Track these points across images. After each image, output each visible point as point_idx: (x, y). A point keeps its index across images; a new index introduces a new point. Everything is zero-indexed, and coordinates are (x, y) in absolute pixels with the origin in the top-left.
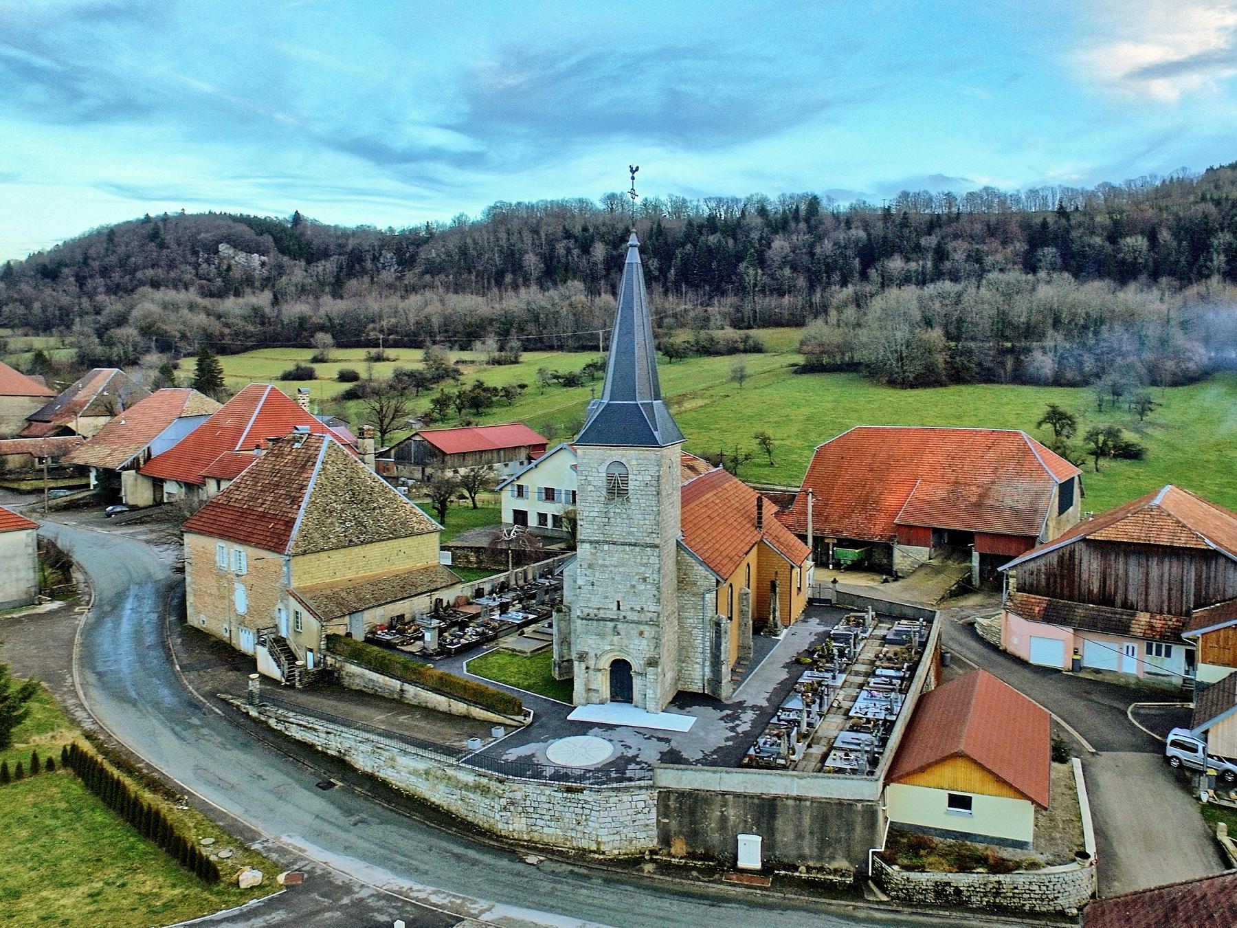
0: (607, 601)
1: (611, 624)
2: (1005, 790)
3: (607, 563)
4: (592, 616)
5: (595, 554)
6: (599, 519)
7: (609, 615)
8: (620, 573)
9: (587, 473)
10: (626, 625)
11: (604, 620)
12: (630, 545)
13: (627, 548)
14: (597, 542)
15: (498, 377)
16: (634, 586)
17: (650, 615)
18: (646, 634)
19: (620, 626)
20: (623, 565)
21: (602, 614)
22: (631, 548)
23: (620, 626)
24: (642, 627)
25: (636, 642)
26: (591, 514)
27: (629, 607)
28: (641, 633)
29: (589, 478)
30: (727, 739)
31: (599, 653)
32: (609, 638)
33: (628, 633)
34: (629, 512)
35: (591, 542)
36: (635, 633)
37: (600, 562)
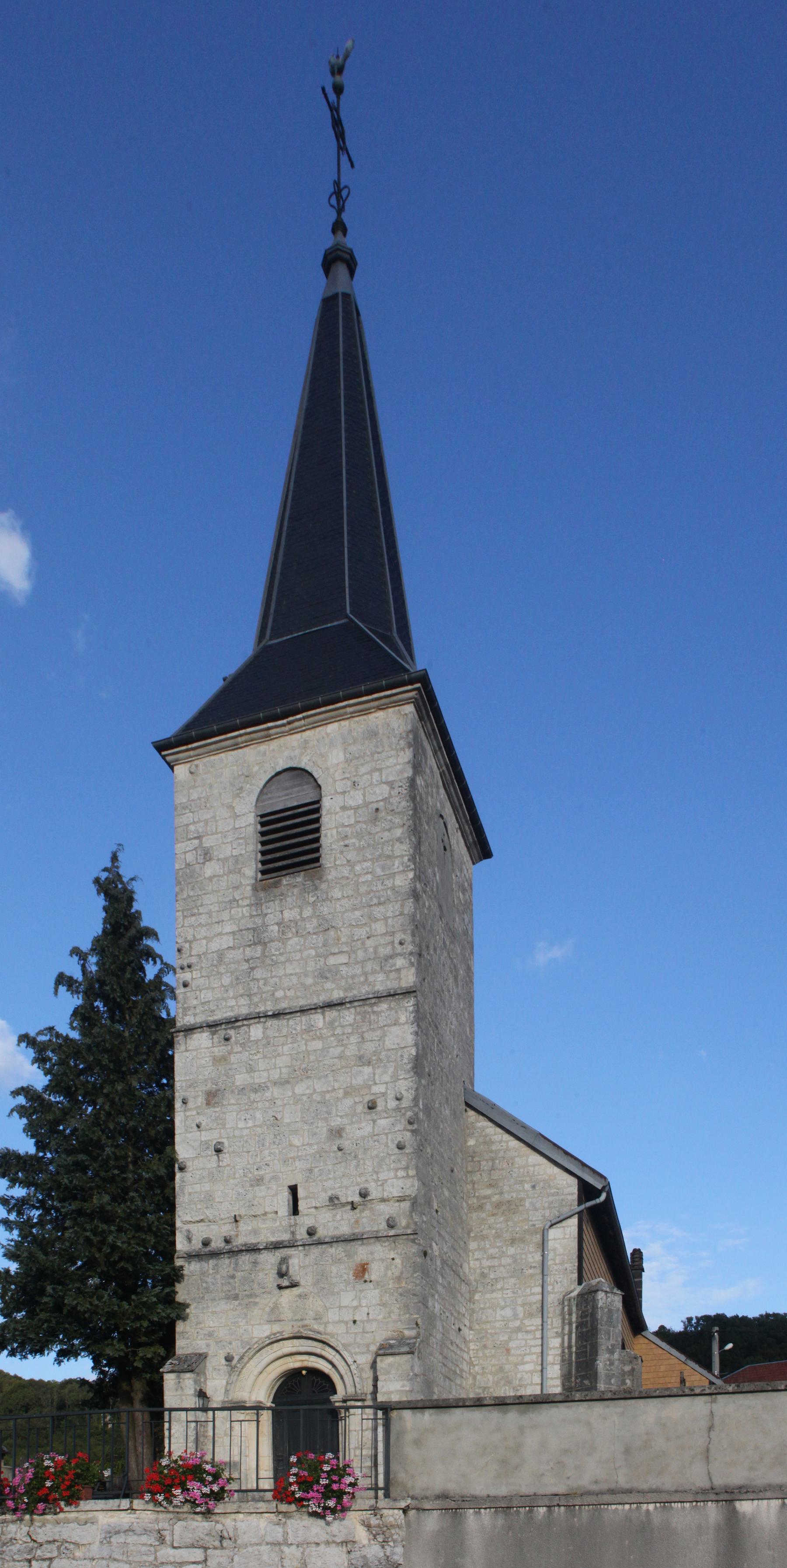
0: (261, 1191)
1: (269, 1260)
2: (448, 1410)
3: (260, 1078)
4: (217, 1244)
5: (224, 1059)
6: (237, 954)
7: (268, 1231)
8: (296, 1099)
9: (200, 827)
10: (315, 1251)
11: (253, 1249)
12: (330, 1005)
13: (318, 1019)
14: (232, 1022)
15: (439, 1336)
16: (338, 1133)
17: (387, 1210)
18: (376, 1271)
19: (297, 1260)
20: (306, 1074)
21: (244, 1236)
22: (331, 1014)
23: (297, 1260)
24: (361, 1252)
25: (348, 1298)
26: (215, 946)
27: (324, 1197)
28: (362, 1271)
29: (208, 842)
30: (78, 998)
31: (237, 1351)
32: (266, 1302)
33: (322, 1277)
34: (325, 909)
35: (213, 1026)
36: (342, 1271)
37: (240, 1079)
